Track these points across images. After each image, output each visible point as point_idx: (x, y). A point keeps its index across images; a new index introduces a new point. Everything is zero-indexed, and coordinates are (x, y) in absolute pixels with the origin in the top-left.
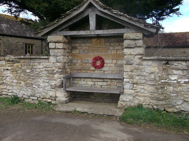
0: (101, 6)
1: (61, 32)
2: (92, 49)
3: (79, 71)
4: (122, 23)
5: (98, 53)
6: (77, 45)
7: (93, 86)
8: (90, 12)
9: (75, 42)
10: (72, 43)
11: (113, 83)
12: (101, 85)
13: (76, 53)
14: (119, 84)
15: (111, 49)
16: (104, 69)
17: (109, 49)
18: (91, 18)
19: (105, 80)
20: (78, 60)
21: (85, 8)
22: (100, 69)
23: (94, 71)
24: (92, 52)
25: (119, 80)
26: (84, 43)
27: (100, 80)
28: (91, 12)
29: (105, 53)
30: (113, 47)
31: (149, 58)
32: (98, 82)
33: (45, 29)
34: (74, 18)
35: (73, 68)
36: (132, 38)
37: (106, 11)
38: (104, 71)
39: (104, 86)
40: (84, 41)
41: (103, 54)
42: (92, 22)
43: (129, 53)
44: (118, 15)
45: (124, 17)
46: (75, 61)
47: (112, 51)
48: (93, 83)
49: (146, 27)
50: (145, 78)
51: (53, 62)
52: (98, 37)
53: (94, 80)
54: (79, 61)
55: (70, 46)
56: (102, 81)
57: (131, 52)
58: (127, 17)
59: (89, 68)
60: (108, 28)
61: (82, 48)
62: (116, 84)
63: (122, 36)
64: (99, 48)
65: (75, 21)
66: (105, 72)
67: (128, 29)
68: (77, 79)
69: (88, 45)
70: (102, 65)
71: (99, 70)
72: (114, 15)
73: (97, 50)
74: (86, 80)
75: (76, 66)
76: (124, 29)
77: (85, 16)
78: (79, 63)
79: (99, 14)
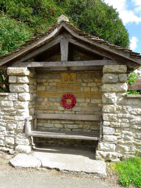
0: (76, 32)
1: (25, 63)
2: (61, 86)
3: (45, 112)
4: (101, 53)
5: (68, 90)
6: (44, 81)
7: (61, 129)
8: (61, 40)
9: (41, 77)
10: (37, 78)
11: (86, 126)
12: (71, 128)
13: (41, 90)
14: (94, 127)
15: (83, 85)
16: (74, 109)
17: (81, 85)
18: (63, 46)
19: (76, 122)
20: (44, 98)
21: (56, 33)
22: (70, 109)
23: (63, 111)
24: (61, 89)
25: (93, 122)
26: (52, 78)
27: (71, 123)
28: (62, 39)
29: (77, 90)
30: (86, 84)
31: (135, 96)
32: (67, 125)
33: (4, 59)
34: (42, 46)
35: (38, 107)
36: (114, 71)
37: (82, 38)
38: (75, 112)
39: (75, 130)
40: (52, 76)
41: (75, 91)
42: (64, 52)
43: (110, 90)
44: (98, 42)
45: (106, 45)
46: (41, 100)
47: (85, 88)
48: (62, 125)
49: (133, 58)
50: (130, 120)
51: (13, 100)
52: (69, 70)
53: (63, 122)
54: (46, 100)
55: (34, 81)
56: (73, 124)
57: (112, 89)
58: (108, 45)
59: (57, 108)
60: (82, 60)
61: (49, 85)
62: (89, 126)
63: (102, 70)
64: (70, 85)
65: (42, 50)
66: (76, 113)
67: (109, 60)
68: (42, 121)
69: (56, 80)
70: (73, 105)
71: (68, 110)
72: (91, 42)
73: (67, 87)
74: (53, 122)
75: (41, 106)
76: (102, 60)
77: (55, 44)
78: (46, 102)
79: (73, 42)
